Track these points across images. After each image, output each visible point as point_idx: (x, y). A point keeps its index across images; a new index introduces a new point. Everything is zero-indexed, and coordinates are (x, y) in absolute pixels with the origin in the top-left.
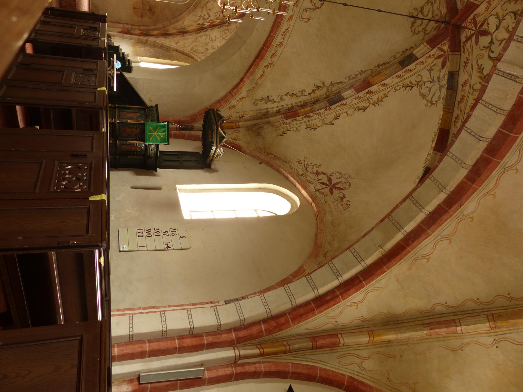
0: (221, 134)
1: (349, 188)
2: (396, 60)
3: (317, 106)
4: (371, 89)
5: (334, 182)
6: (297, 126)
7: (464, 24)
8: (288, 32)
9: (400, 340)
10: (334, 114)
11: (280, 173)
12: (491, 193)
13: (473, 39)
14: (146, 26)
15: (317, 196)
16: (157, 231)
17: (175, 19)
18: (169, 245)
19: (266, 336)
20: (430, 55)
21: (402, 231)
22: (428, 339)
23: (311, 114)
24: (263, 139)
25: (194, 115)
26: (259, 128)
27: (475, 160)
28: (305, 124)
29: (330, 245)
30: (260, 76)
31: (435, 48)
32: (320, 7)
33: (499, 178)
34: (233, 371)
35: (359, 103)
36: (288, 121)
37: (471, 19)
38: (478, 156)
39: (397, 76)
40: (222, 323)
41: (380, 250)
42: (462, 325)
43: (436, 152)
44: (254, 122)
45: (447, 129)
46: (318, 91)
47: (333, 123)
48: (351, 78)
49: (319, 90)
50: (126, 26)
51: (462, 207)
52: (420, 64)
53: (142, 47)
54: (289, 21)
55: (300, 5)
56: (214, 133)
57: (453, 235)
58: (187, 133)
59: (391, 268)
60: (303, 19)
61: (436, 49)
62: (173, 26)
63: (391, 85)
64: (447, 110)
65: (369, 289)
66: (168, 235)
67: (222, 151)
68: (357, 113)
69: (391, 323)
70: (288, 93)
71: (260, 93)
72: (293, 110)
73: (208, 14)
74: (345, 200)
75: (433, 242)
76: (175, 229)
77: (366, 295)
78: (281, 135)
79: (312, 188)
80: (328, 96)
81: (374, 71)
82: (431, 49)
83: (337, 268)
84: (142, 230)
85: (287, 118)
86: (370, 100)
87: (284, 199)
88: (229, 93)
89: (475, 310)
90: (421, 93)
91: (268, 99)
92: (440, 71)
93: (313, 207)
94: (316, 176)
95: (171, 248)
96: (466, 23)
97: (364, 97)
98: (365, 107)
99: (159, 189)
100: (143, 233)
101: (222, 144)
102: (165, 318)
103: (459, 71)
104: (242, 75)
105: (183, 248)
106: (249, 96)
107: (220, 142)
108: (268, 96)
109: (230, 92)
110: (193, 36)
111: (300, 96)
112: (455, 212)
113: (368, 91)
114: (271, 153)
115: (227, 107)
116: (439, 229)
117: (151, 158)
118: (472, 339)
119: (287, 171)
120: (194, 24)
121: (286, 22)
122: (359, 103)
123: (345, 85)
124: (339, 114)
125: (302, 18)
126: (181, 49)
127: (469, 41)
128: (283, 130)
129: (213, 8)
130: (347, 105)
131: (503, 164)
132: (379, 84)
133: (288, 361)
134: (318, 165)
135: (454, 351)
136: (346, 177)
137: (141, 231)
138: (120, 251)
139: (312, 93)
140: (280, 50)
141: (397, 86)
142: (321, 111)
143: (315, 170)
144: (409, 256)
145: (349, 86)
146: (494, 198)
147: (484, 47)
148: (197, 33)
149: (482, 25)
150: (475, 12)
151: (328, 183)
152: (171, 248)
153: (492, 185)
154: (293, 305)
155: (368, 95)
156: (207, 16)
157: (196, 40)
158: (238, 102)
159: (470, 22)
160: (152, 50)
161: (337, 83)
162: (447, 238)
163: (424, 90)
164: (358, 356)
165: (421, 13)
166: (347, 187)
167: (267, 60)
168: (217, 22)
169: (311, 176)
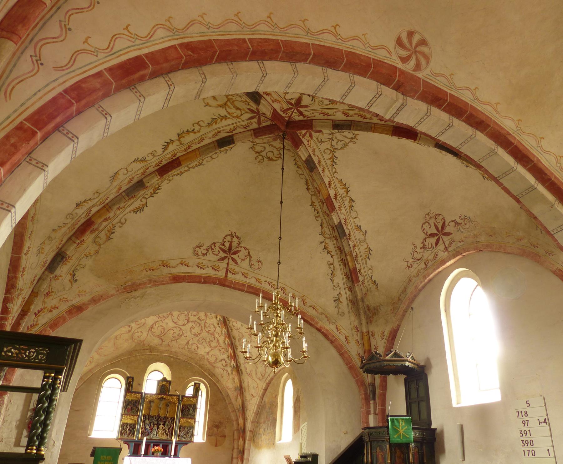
0: (392, 357)
1: (443, 216)
2: (305, 173)
3: (347, 249)
4: (332, 195)
5: (435, 231)
6: (366, 269)
7: (286, 119)
8: (271, 282)
10: (355, 231)
11: (423, 287)
12: (495, 107)
13: (301, 110)
14: (234, 433)
15: (454, 250)
17: (226, 398)
18: (542, 420)
20: (308, 144)
21: (536, 186)
23: (354, 254)
24: (382, 305)
26: (369, 309)
27: (468, 127)
28: (364, 261)
29: (520, 240)
30: (315, 310)
31: (302, 141)
32: (248, 250)
33: (483, 103)
35: (345, 207)
36: (361, 279)
37: (284, 113)
39: (323, 172)
41: (556, 206)
43: (418, 138)
45: (393, 128)
46: (329, 248)
48: (318, 215)
49: (328, 247)
50: (235, 455)
51: (511, 133)
52: (315, 151)
53: (261, 437)
54: (262, 281)
55: (246, 272)
56: (392, 364)
57: (536, 136)
58: (378, 391)
60: (259, 267)
61: (303, 140)
62: (233, 401)
63: (330, 176)
64: (373, 129)
66: (528, 421)
70: (330, 279)
71: (331, 309)
72: (349, 273)
73: (221, 361)
74: (459, 221)
75: (544, 154)
76: (518, 412)
78: (377, 286)
79: (442, 255)
80: (334, 238)
81: (313, 193)
82: (302, 144)
84: (524, 451)
85: (358, 280)
86: (343, 196)
87: (457, 285)
88: (333, 344)
90: (341, 149)
91: (337, 300)
92: (323, 134)
93: (468, 255)
94: (427, 249)
95: (545, 419)
96: (286, 116)
98: (350, 200)
99: (462, 427)
100: (529, 450)
103: (332, 120)
105: (544, 404)
106: (334, 321)
109: (332, 343)
110: (245, 377)
112: (515, 138)
113: (334, 198)
114: (399, 297)
115: (347, 345)
116: (532, 151)
117: (423, 435)
119: (422, 280)
120: (231, 377)
121: (262, 285)
122: (345, 207)
123: (324, 221)
124: (355, 226)
125: (258, 269)
127: (304, 113)
128: (371, 284)
129: (215, 355)
130: (347, 218)
131: (471, 102)
132: (328, 188)
134: (413, 247)
136: (428, 218)
137: (527, 453)
139: (331, 255)
141: (332, 170)
142: (351, 244)
143: (419, 250)
144: (559, 176)
145: (326, 217)
147: (312, 101)
148: (242, 373)
149: (291, 104)
150: (279, 111)
151: (437, 237)
152: (545, 419)
153: (489, 108)
155: (338, 198)
156: (224, 362)
157: (250, 375)
158: (341, 333)
159: (286, 114)
160: (263, 426)
161: (322, 228)
162: (539, 142)
163: (340, 145)
165: (261, 153)
166: (441, 217)
168: (231, 351)
169: (428, 255)
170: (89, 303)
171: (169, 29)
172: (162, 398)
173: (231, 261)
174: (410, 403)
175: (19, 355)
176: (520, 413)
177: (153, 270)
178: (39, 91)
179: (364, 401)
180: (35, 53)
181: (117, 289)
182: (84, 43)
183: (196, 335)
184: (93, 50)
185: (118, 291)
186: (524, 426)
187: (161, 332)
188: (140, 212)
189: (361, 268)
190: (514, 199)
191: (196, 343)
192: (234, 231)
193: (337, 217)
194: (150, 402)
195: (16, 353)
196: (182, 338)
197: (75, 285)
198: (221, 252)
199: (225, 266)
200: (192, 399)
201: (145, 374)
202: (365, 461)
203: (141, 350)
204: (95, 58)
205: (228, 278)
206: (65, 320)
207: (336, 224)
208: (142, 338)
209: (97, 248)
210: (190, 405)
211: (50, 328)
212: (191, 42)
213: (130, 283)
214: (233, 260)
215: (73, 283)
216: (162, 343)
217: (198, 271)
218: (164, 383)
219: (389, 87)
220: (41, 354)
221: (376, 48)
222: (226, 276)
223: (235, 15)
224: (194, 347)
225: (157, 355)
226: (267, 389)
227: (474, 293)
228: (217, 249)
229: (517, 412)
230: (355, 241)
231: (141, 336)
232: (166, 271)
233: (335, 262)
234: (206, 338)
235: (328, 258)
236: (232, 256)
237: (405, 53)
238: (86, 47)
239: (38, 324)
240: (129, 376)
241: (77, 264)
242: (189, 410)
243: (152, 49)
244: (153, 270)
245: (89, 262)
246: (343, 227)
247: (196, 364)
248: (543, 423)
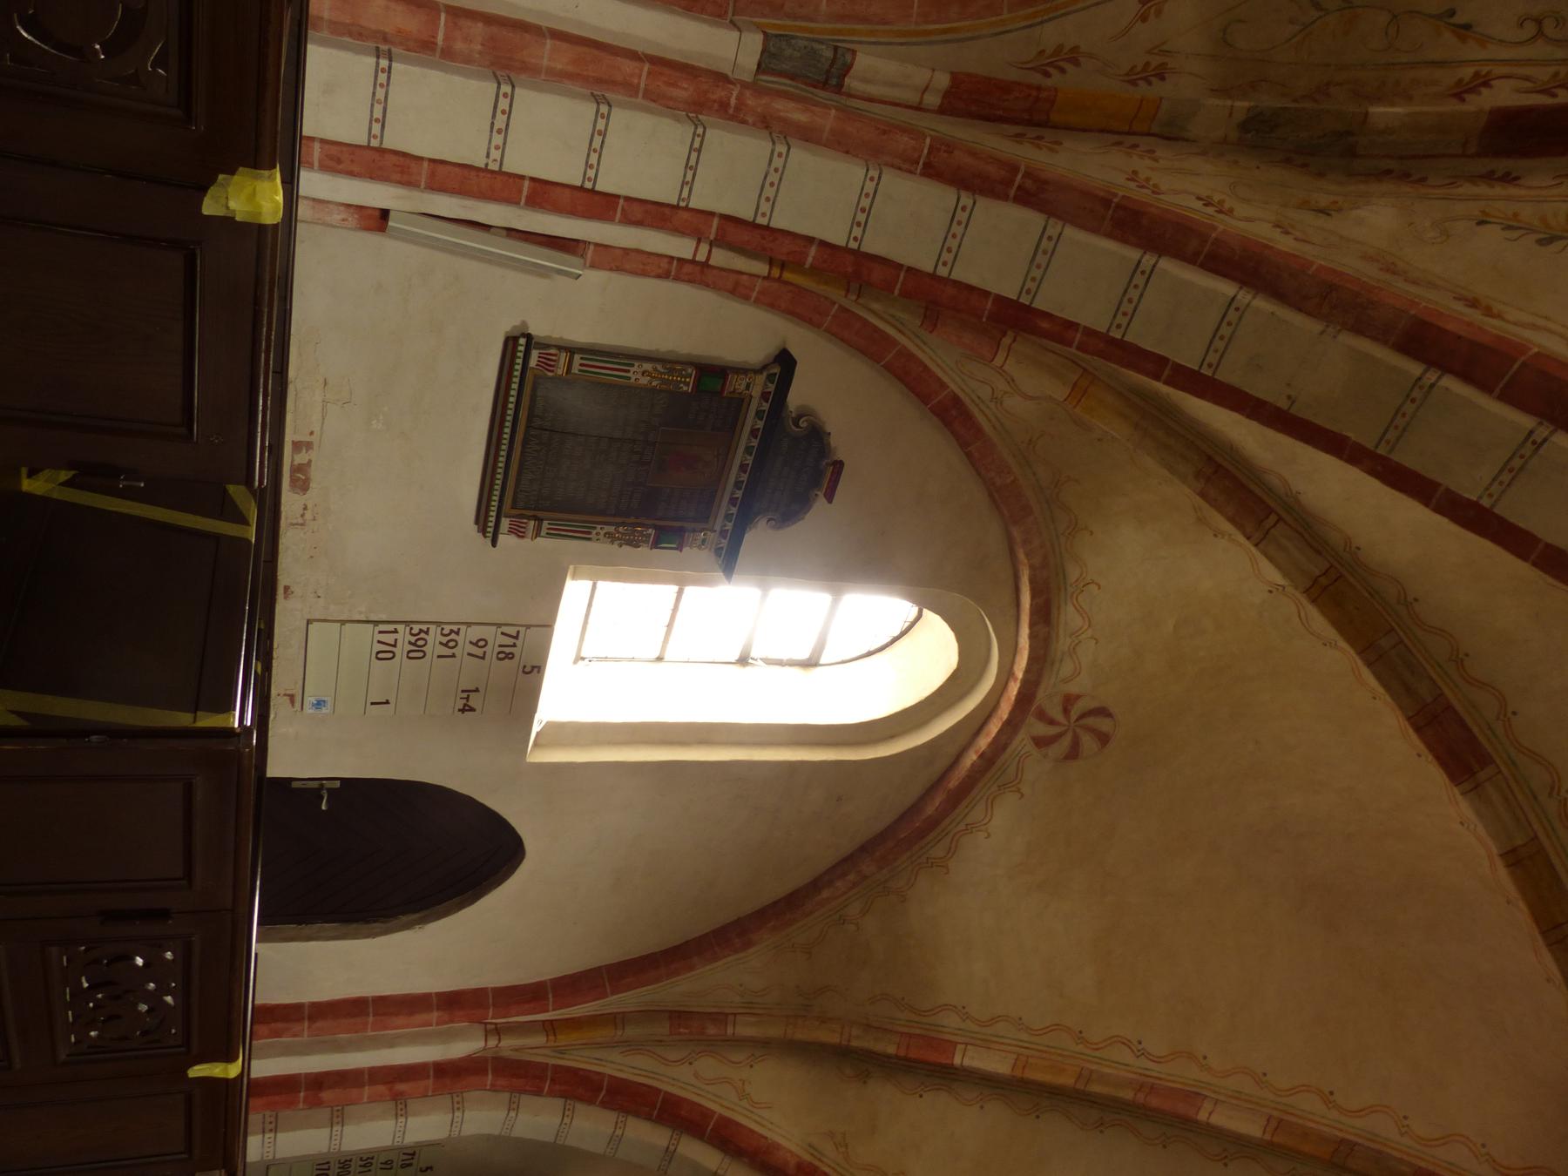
16: (449, 638)
42: (1260, 546)
66: (483, 658)
83: (1141, 307)
100: (395, 646)
102: (509, 118)
138: (309, 622)
176: (513, 641)
186: (471, 642)
190: (1372, 472)
202: (257, 483)
248: (465, 701)
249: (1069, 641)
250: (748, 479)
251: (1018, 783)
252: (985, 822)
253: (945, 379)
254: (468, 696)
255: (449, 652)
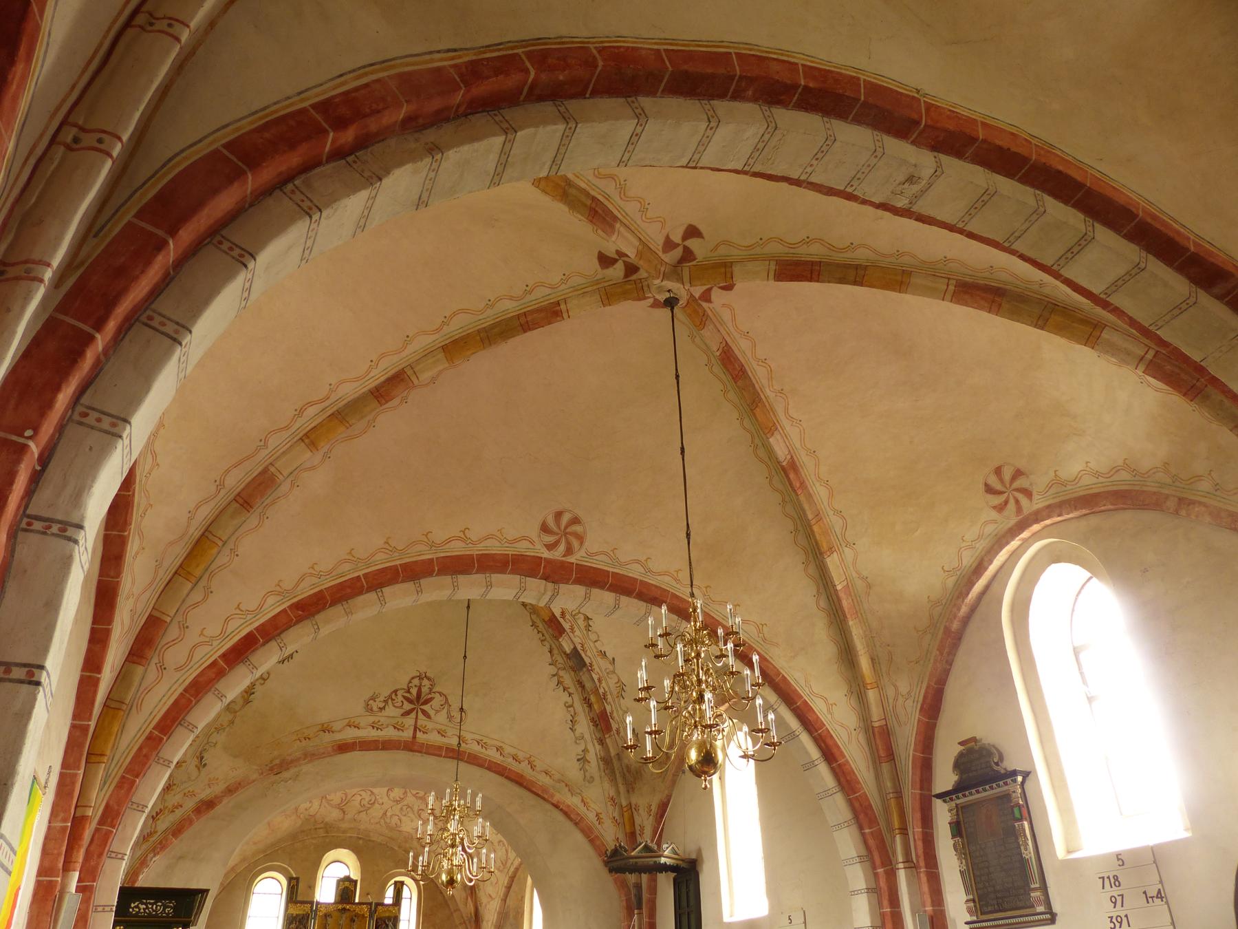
3: (588, 685)
8: (481, 740)
9: (868, 646)
12: (676, 575)
19: (879, 825)
22: (861, 614)
23: (601, 691)
25: (616, 883)
26: (629, 771)
30: (548, 777)
34: (924, 871)
35: (579, 628)
38: (636, 600)
40: (865, 887)
44: (620, 780)
47: (611, 660)
55: (444, 728)
58: (645, 896)
59: (778, 670)
62: (461, 906)
65: (808, 693)
66: (1122, 896)
67: (667, 845)
68: (594, 628)
69: (850, 658)
70: (570, 728)
71: (574, 773)
72: (596, 719)
77: (817, 695)
86: (573, 613)
89: (816, 565)
91: (583, 760)
95: (1159, 889)
97: (570, 621)
101: (656, 848)
104: (549, 806)
106: (579, 792)
107: (655, 852)
108: (578, 760)
109: (576, 824)
111: (574, 711)
118: (852, 568)
121: (468, 746)
122: (579, 628)
123: (553, 646)
126: (502, 891)
133: (910, 793)
135: (869, 586)
140: (508, 750)
142: (595, 677)
146: (680, 570)
152: (1159, 889)
153: (667, 579)
154: (837, 790)
155: (568, 617)
161: (552, 655)
164: (896, 699)
167: (523, 768)
170: (223, 794)
171: (279, 594)
172: (344, 909)
173: (420, 714)
174: (680, 915)
175: (147, 911)
176: (1106, 878)
177: (309, 738)
178: (164, 696)
179: (625, 911)
180: (159, 660)
181: (260, 771)
182: (200, 635)
183: (397, 801)
184: (207, 640)
185: (262, 773)
186: (1115, 907)
187: (342, 799)
188: (288, 661)
189: (613, 711)
191: (397, 814)
192: (423, 669)
193: (569, 642)
194: (326, 916)
195: (144, 909)
196: (374, 807)
197: (204, 771)
198: (405, 702)
199: (412, 722)
200: (391, 909)
201: (318, 870)
203: (310, 830)
204: (210, 648)
205: (418, 740)
206: (191, 822)
207: (568, 652)
208: (312, 812)
209: (230, 717)
210: (389, 918)
211: (173, 835)
212: (300, 600)
213: (277, 761)
214: (425, 713)
215: (201, 769)
216: (344, 817)
217: (373, 734)
218: (347, 884)
219: (536, 578)
220: (168, 907)
221: (516, 541)
222: (414, 737)
223: (348, 554)
224: (395, 820)
225: (337, 837)
226: (511, 885)
227: (1083, 591)
228: (400, 698)
229: (1100, 878)
230: (600, 672)
231: (310, 807)
232: (327, 738)
233: (575, 702)
234: (413, 805)
235: (565, 697)
236: (422, 707)
237: (550, 539)
238: (202, 639)
239: (157, 832)
240: (294, 876)
241: (205, 742)
242: (387, 926)
243: (262, 621)
244: (309, 738)
245: (221, 738)
246: (580, 655)
247: (399, 847)
248: (1155, 899)
249: (977, 545)
250: (1008, 778)
251: (1053, 480)
252: (1084, 472)
253: (916, 721)
254: (1150, 897)
255: (1125, 920)
